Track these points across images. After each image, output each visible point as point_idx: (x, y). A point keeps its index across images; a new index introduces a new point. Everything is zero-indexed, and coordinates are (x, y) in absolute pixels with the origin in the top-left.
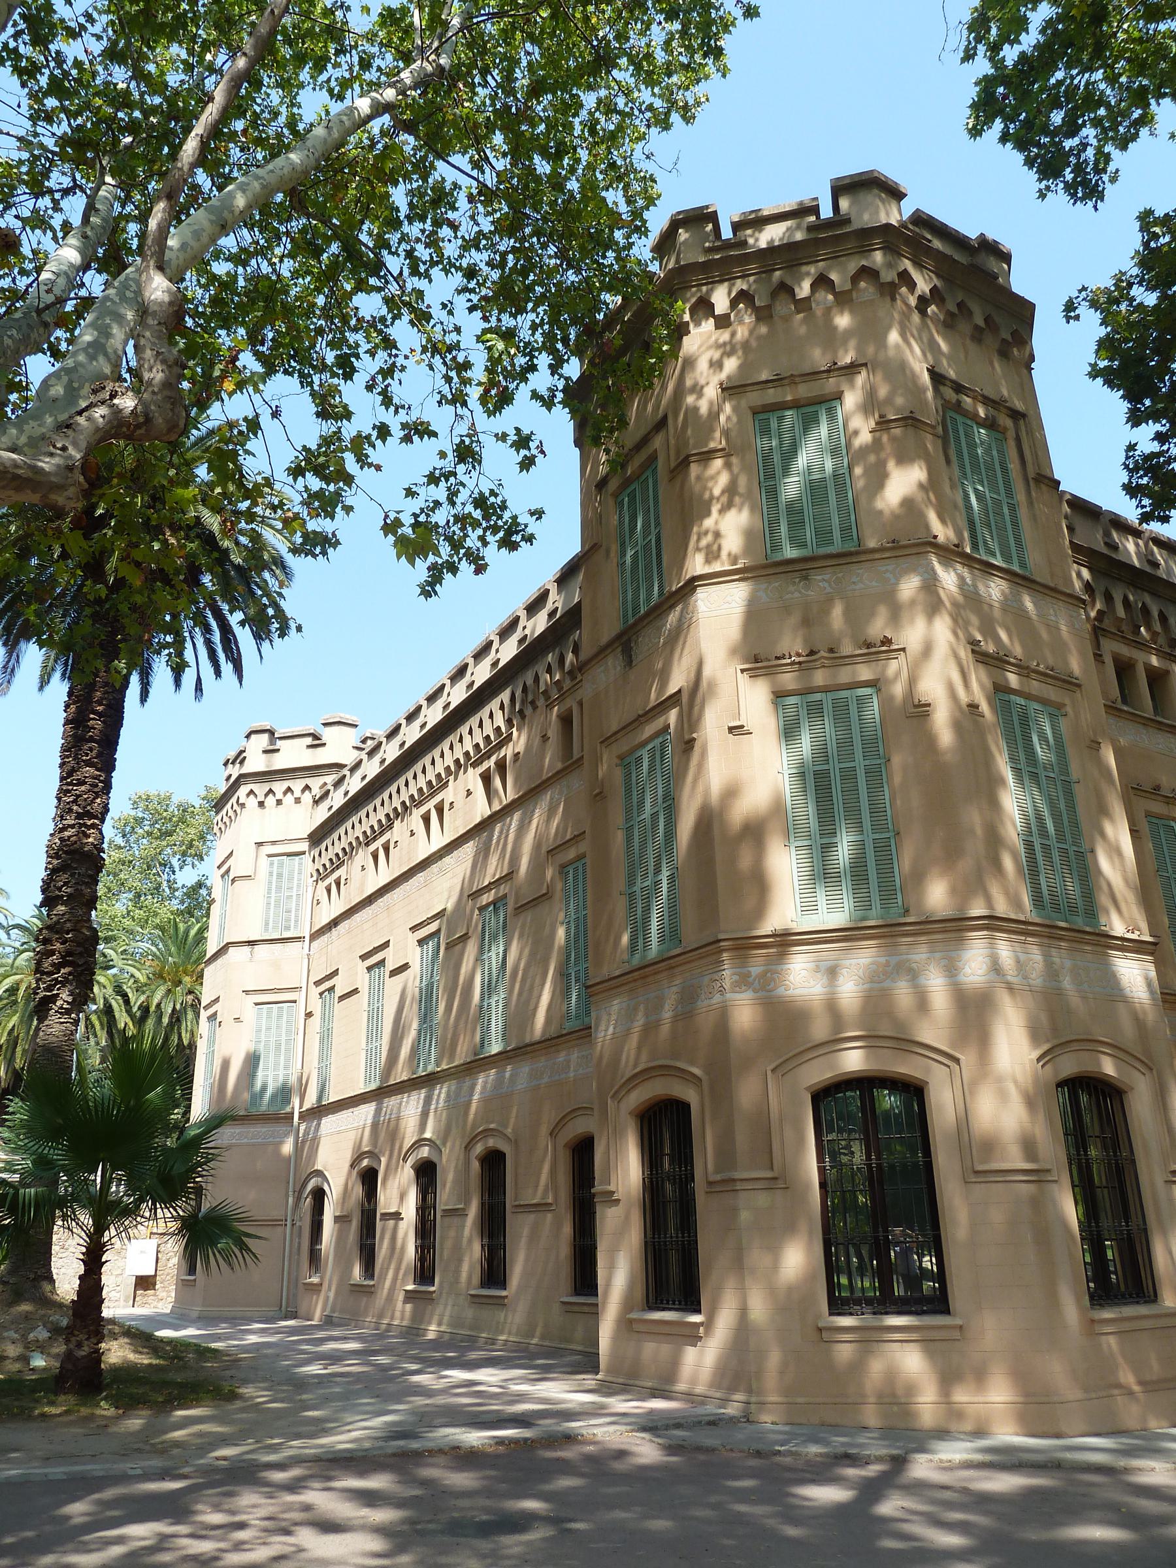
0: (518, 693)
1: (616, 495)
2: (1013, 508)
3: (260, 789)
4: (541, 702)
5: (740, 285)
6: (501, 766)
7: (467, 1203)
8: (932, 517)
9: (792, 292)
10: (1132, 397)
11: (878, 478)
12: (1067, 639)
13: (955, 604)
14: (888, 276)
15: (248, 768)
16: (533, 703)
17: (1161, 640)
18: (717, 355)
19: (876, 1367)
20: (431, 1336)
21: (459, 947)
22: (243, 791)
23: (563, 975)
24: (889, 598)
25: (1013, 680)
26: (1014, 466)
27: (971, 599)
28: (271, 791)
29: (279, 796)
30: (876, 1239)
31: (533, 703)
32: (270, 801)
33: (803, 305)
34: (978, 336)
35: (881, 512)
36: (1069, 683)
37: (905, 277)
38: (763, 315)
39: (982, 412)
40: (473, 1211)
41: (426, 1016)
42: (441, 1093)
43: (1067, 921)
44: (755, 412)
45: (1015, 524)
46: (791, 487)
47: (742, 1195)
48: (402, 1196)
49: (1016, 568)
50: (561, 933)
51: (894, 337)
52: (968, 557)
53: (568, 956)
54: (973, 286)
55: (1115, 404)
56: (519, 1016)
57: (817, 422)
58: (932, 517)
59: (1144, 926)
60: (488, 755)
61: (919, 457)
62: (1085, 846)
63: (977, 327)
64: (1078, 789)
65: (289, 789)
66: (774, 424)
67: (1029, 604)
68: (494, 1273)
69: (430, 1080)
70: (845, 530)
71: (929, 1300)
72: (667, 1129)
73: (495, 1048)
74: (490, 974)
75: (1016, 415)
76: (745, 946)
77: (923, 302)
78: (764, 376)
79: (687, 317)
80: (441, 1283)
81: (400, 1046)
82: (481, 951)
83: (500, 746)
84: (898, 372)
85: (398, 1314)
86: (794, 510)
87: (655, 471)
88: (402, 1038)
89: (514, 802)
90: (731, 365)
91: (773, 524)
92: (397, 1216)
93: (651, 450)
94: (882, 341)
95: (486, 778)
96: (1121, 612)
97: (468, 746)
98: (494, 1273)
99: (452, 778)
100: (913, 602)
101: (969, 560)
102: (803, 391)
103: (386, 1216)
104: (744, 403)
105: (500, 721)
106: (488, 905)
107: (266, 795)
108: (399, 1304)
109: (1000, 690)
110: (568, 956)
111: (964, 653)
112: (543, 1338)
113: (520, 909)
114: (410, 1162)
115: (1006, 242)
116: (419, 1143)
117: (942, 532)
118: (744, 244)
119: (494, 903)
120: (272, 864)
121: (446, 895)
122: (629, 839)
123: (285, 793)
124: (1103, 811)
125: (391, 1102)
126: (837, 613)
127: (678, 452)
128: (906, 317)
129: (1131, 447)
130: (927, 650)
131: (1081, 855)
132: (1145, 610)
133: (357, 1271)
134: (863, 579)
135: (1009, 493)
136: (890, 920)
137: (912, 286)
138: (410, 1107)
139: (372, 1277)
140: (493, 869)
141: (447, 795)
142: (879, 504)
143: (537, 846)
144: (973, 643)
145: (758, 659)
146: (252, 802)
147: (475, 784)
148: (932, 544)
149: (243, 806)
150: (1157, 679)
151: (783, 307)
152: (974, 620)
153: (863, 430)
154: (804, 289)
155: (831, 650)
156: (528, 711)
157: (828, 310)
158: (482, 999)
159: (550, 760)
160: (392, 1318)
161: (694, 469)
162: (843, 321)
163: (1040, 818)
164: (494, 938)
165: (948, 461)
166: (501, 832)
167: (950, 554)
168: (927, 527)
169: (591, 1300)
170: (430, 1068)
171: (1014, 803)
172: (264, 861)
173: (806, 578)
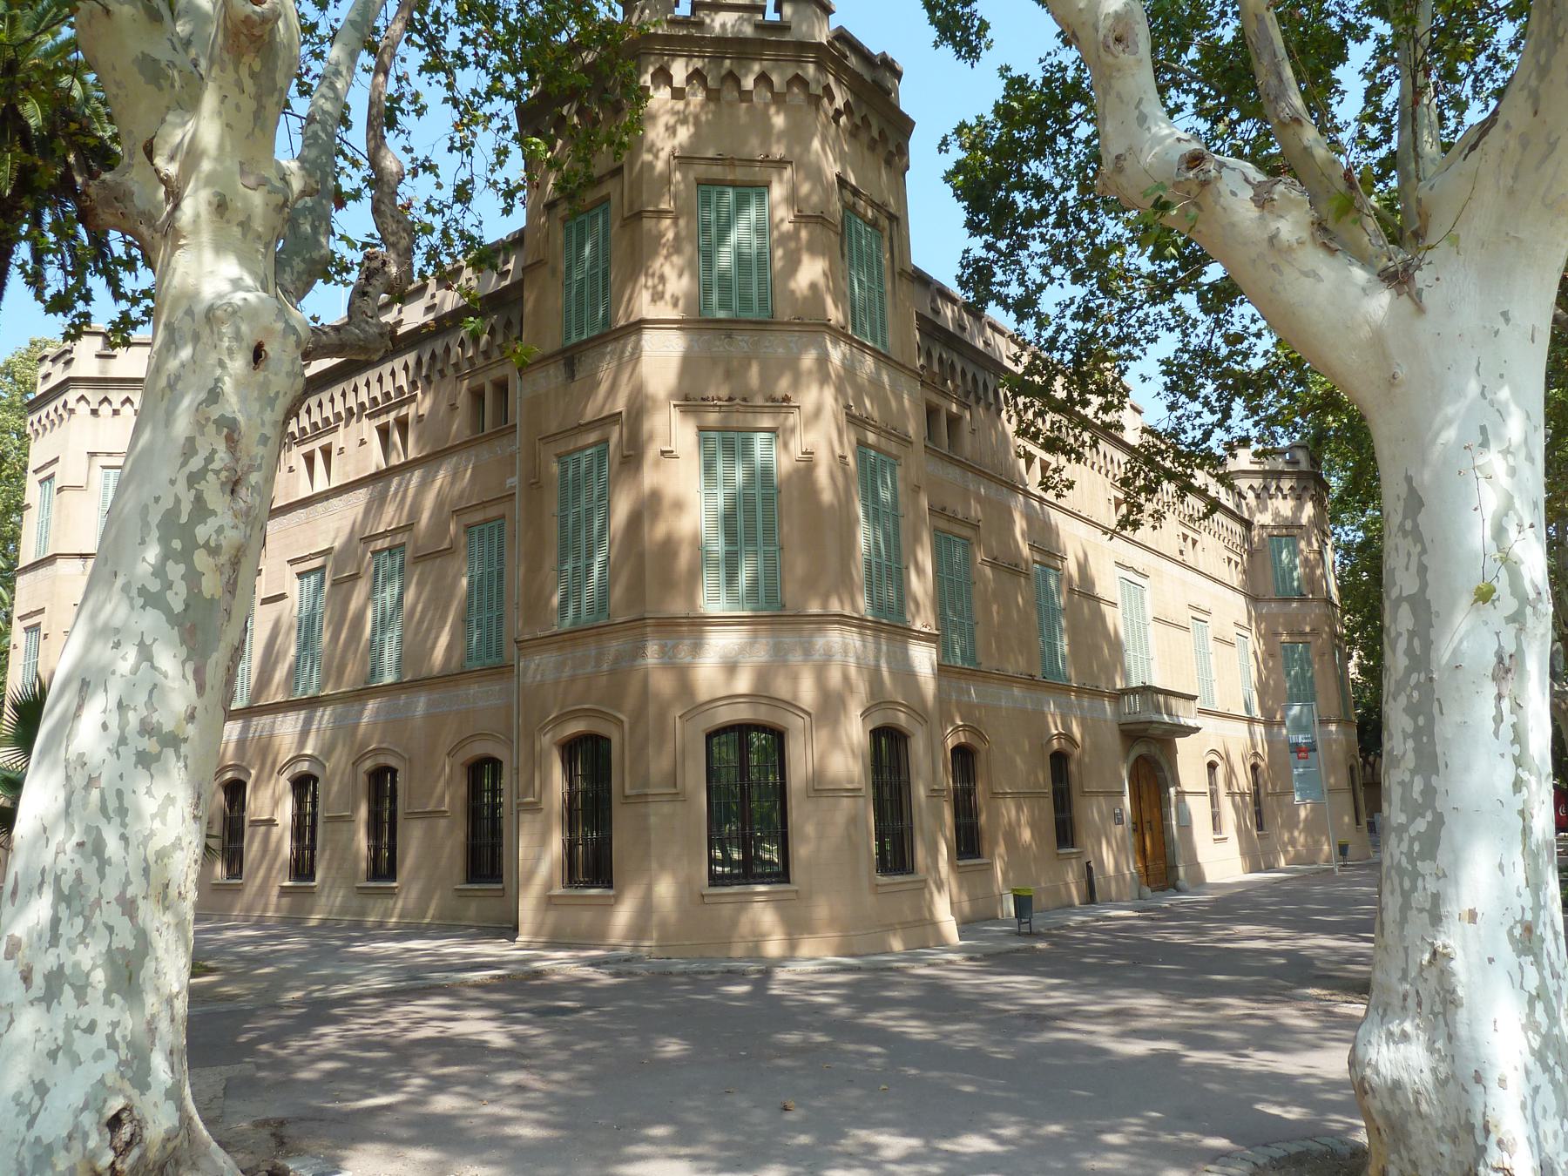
0: (426, 359)
1: (564, 220)
2: (881, 296)
3: (94, 396)
4: (450, 372)
5: (698, 63)
6: (402, 424)
7: (355, 809)
8: (829, 301)
9: (737, 82)
10: (973, 209)
11: (793, 264)
12: (908, 405)
13: (838, 376)
14: (816, 89)
15: (74, 371)
16: (441, 372)
17: (960, 391)
18: (672, 121)
19: (745, 919)
20: (312, 923)
21: (345, 586)
22: (71, 396)
23: (464, 620)
24: (792, 365)
25: (871, 437)
26: (886, 261)
27: (850, 369)
28: (106, 399)
29: (116, 405)
30: (744, 836)
31: (441, 372)
32: (105, 410)
33: (745, 96)
34: (872, 145)
35: (793, 292)
36: (905, 441)
37: (827, 89)
38: (712, 96)
39: (870, 214)
40: (363, 812)
41: (306, 644)
42: (325, 716)
43: (890, 624)
44: (699, 183)
45: (882, 309)
46: (725, 258)
47: (652, 806)
48: (276, 803)
49: (878, 347)
50: (464, 582)
51: (816, 144)
52: (850, 338)
53: (470, 605)
54: (871, 88)
55: (958, 212)
56: (412, 653)
57: (748, 202)
58: (829, 301)
59: (933, 623)
60: (387, 410)
61: (824, 255)
62: (904, 564)
63: (873, 139)
64: (901, 520)
65: (128, 400)
66: (714, 198)
67: (885, 379)
68: (384, 867)
69: (311, 703)
70: (762, 300)
71: (777, 875)
72: (589, 756)
73: (389, 678)
74: (384, 609)
75: (893, 218)
76: (669, 625)
77: (838, 113)
78: (710, 154)
79: (649, 84)
80: (324, 881)
81: (273, 670)
82: (373, 590)
83: (401, 404)
84: (816, 174)
85: (272, 907)
86: (724, 282)
87: (605, 212)
88: (276, 662)
89: (415, 460)
90: (684, 134)
91: (706, 290)
92: (270, 823)
93: (604, 192)
94: (807, 148)
95: (384, 432)
96: (936, 368)
97: (364, 397)
98: (384, 867)
99: (342, 424)
100: (810, 372)
101: (849, 339)
102: (739, 174)
103: (256, 823)
104: (691, 176)
105: (402, 380)
106: (382, 550)
107: (101, 403)
108: (274, 899)
109: (862, 443)
110: (470, 605)
111: (843, 418)
112: (401, 917)
113: (418, 559)
114: (287, 775)
115: (901, 63)
116: (298, 758)
117: (835, 314)
118: (700, 24)
119: (390, 549)
120: (107, 476)
121: (332, 535)
122: (563, 526)
123: (123, 403)
124: (917, 539)
125: (260, 723)
126: (754, 371)
127: (631, 204)
128: (825, 127)
129: (967, 251)
130: (818, 412)
131: (899, 570)
132: (952, 366)
133: (219, 870)
134: (776, 345)
135: (881, 284)
136: (775, 613)
137: (832, 99)
138: (287, 728)
139: (239, 875)
140: (389, 518)
141: (338, 439)
142: (792, 285)
143: (439, 505)
144: (848, 407)
145: (689, 402)
146: (83, 409)
147: (370, 434)
148: (826, 326)
149: (72, 411)
150: (954, 421)
151: (730, 94)
152: (850, 391)
153: (784, 215)
154: (748, 83)
155: (745, 400)
156: (435, 377)
157: (767, 106)
158: (374, 633)
159: (459, 427)
160: (265, 910)
161: (648, 224)
162: (779, 121)
163: (876, 543)
164: (388, 578)
165: (843, 255)
166: (399, 485)
167: (839, 334)
168: (824, 310)
169: (499, 886)
170: (311, 693)
171: (863, 537)
172: (98, 473)
173: (729, 336)
